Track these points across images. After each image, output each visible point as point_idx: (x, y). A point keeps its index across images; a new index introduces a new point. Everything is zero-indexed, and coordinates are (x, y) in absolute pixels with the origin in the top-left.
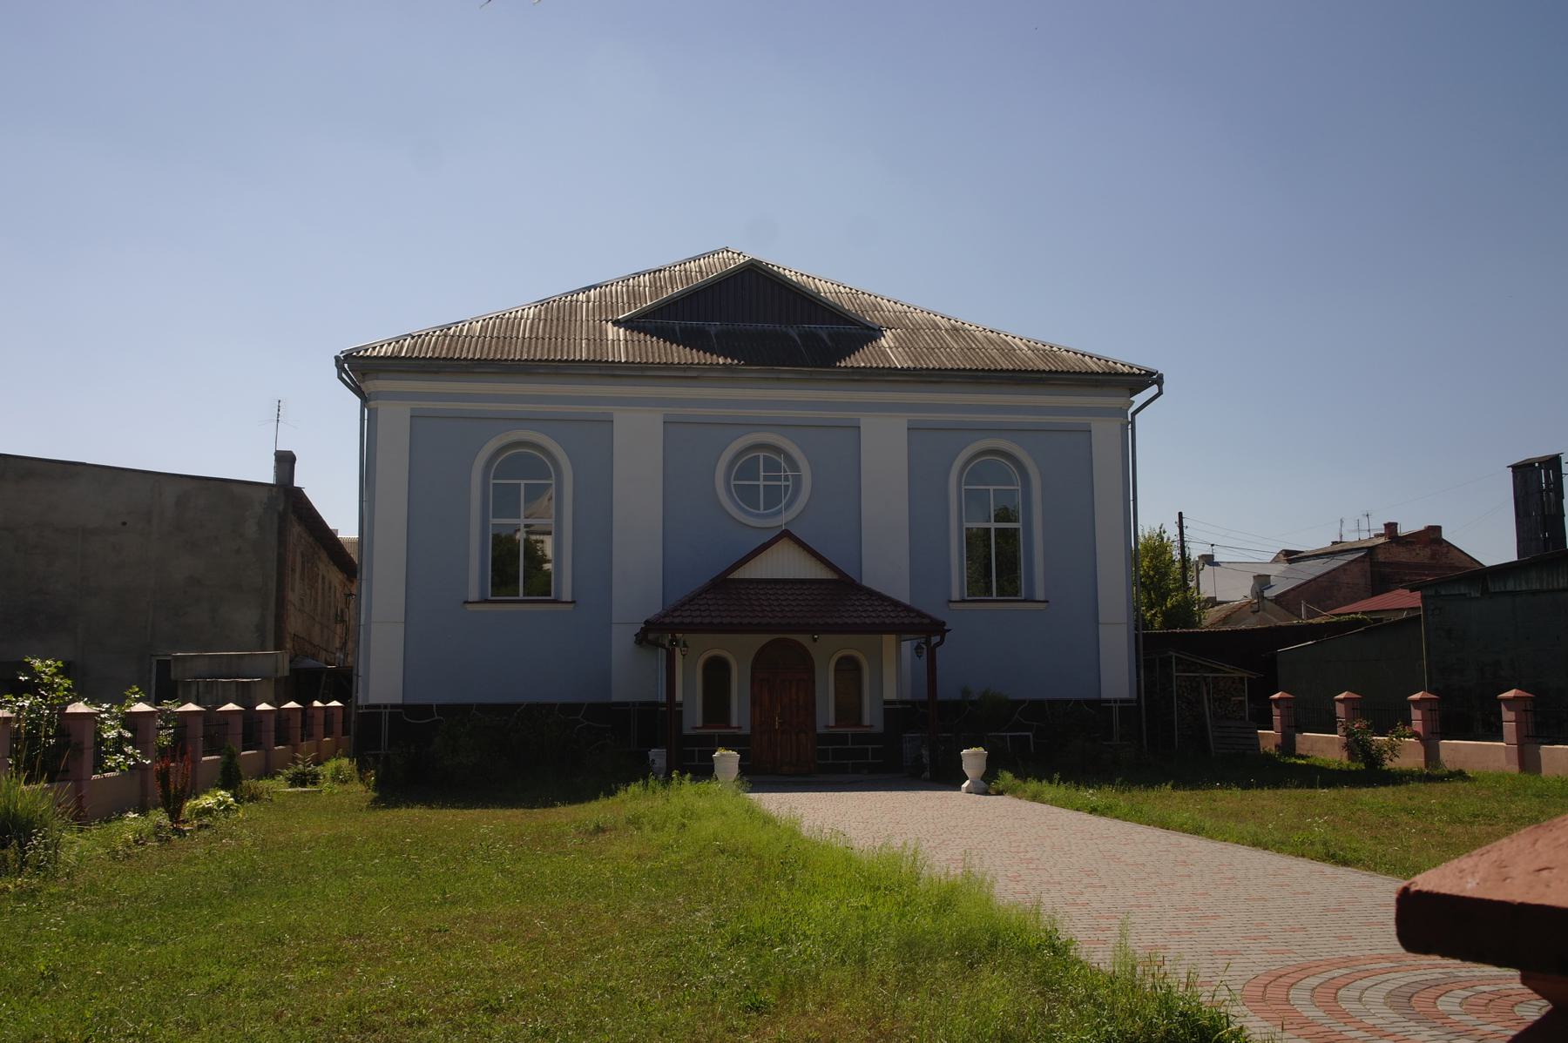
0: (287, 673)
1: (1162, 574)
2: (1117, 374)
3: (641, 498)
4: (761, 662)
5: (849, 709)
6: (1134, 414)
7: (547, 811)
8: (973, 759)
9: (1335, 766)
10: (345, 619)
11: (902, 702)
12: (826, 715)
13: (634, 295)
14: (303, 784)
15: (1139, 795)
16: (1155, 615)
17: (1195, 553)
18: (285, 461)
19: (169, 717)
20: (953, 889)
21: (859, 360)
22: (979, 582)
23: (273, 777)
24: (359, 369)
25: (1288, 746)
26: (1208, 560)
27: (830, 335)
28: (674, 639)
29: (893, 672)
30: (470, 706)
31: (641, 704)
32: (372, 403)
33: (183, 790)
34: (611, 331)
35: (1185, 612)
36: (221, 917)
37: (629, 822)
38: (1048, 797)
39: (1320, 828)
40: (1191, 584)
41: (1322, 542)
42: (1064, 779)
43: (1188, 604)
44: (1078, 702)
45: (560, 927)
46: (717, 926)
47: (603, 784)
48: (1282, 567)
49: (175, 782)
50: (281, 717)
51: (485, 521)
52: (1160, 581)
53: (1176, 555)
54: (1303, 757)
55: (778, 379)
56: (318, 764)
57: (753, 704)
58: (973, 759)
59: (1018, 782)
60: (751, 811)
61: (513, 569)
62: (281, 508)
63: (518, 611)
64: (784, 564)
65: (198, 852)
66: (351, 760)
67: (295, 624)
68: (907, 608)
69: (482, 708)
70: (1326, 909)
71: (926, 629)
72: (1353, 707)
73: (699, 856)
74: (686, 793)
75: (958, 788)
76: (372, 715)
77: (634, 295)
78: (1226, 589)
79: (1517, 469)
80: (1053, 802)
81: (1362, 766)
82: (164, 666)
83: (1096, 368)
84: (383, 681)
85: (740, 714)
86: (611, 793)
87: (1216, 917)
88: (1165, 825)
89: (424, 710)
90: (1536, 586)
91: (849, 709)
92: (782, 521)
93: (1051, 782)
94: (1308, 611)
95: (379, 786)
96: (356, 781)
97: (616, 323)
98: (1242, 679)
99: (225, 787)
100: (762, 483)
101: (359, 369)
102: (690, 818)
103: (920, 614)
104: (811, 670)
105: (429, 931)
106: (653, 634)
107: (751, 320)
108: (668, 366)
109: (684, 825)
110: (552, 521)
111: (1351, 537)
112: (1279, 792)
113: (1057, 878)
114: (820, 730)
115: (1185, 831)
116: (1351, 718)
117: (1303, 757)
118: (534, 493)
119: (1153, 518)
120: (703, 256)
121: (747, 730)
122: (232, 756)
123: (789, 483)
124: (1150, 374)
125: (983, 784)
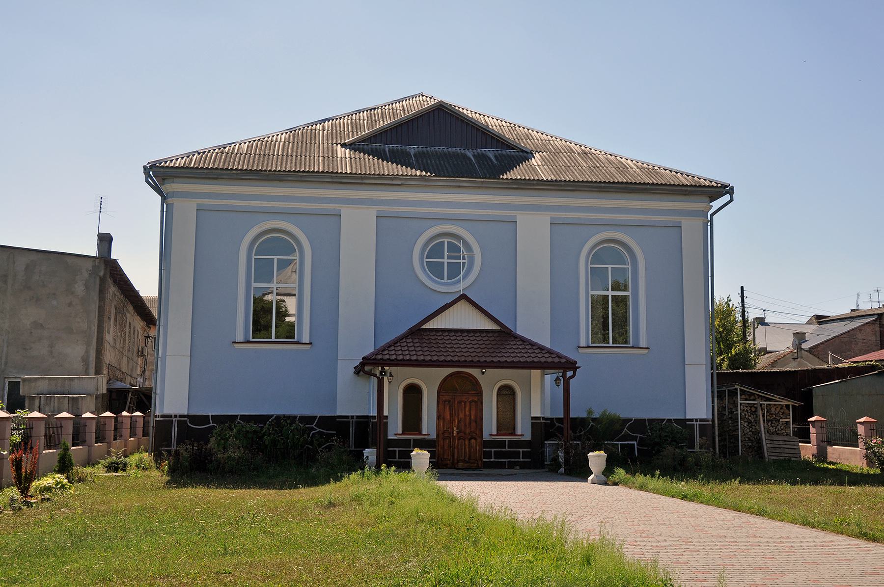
0: (105, 392)
1: (729, 332)
2: (700, 186)
3: (362, 268)
4: (444, 388)
5: (507, 424)
7: (292, 492)
8: (596, 459)
9: (858, 471)
10: (146, 353)
11: (544, 418)
12: (490, 428)
13: (356, 126)
14: (116, 470)
15: (717, 488)
16: (723, 359)
17: (751, 315)
18: (105, 240)
19: (20, 421)
20: (592, 548)
21: (515, 174)
23: (93, 465)
24: (159, 175)
25: (822, 455)
26: (761, 321)
27: (496, 157)
28: (383, 371)
29: (538, 398)
30: (235, 417)
31: (358, 417)
32: (170, 200)
33: (31, 473)
34: (340, 151)
35: (743, 359)
36: (64, 563)
37: (352, 499)
38: (651, 487)
39: (854, 514)
40: (749, 338)
41: (845, 311)
42: (663, 475)
43: (747, 352)
44: (669, 421)
45: (311, 571)
46: (424, 572)
47: (333, 473)
48: (814, 327)
49: (26, 467)
50: (101, 425)
51: (587, 293)
52: (726, 335)
53: (739, 317)
54: (833, 464)
55: (459, 187)
56: (126, 456)
57: (438, 418)
58: (596, 459)
59: (629, 476)
60: (439, 492)
61: (265, 319)
62: (102, 274)
63: (271, 350)
64: (462, 318)
65: (44, 517)
66: (150, 454)
67: (109, 357)
68: (550, 352)
69: (244, 418)
70: (864, 573)
71: (565, 366)
72: (873, 430)
73: (405, 524)
74: (392, 478)
75: (587, 481)
76: (165, 423)
77: (356, 126)
78: (773, 345)
80: (655, 491)
81: (878, 471)
82: (14, 386)
83: (685, 182)
84: (173, 400)
85: (429, 426)
86: (338, 479)
87: (782, 574)
88: (737, 509)
89: (204, 419)
91: (507, 424)
92: (460, 288)
93: (653, 476)
94: (833, 359)
95: (172, 471)
96: (154, 468)
97: (344, 145)
98: (787, 406)
99: (61, 471)
100: (446, 260)
101: (159, 175)
102: (396, 497)
103: (559, 356)
104: (480, 394)
105: (218, 573)
106: (365, 367)
107: (441, 143)
108: (381, 176)
109: (393, 503)
110: (296, 285)
111: (865, 307)
112: (818, 488)
113: (663, 544)
114: (486, 437)
115: (752, 513)
116: (869, 436)
117: (833, 464)
118: (283, 265)
119: (724, 291)
120: (405, 99)
121: (433, 437)
122: (66, 449)
123: (466, 261)
124: (724, 186)
125: (603, 478)
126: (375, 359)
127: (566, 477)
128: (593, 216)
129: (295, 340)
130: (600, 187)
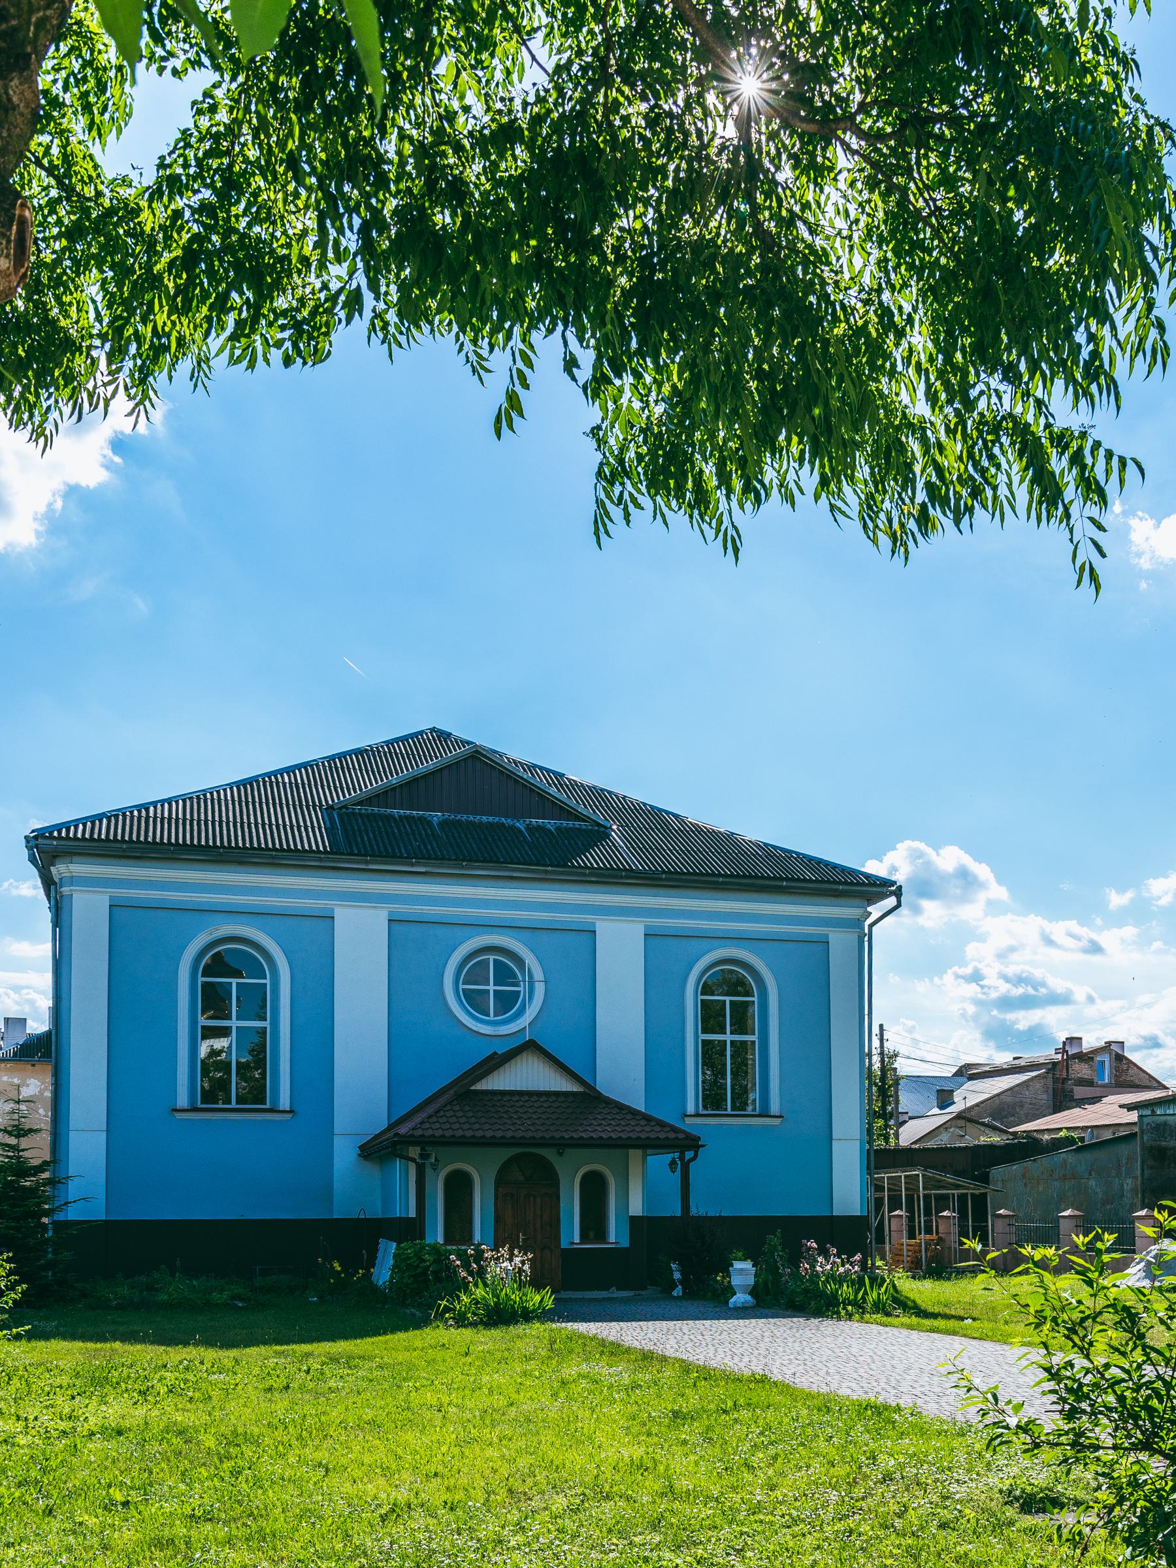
6: (871, 926)
21: (593, 858)
22: (712, 1099)
51: (696, 1037)
55: (512, 878)
64: (529, 1076)
71: (684, 1145)
91: (594, 1222)
104: (555, 1183)
107: (449, 811)
126: (412, 1135)
129: (268, 1106)
130: (717, 883)
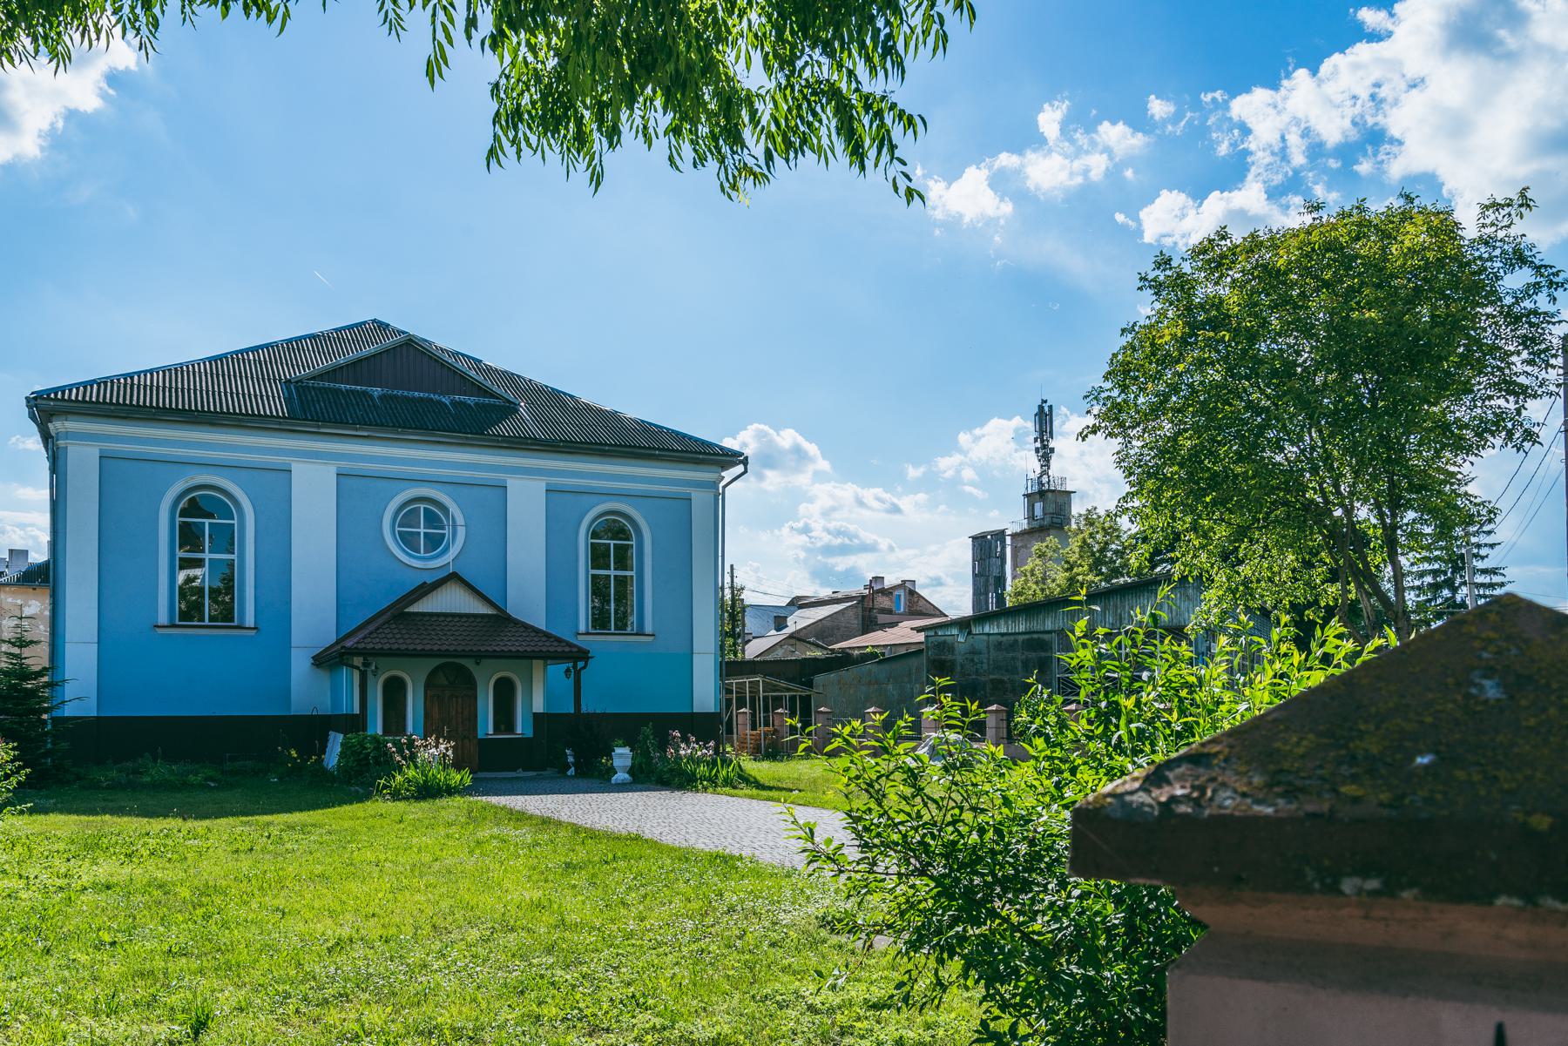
12: (486, 726)
22: (600, 621)
29: (539, 695)
64: (452, 601)
68: (548, 636)
79: (974, 538)
90: (1003, 630)
91: (504, 716)
100: (422, 530)
101: (48, 409)
107: (387, 387)
127: (583, 783)
128: (595, 483)
129: (236, 623)
